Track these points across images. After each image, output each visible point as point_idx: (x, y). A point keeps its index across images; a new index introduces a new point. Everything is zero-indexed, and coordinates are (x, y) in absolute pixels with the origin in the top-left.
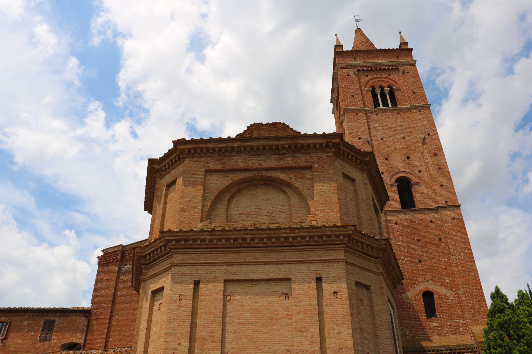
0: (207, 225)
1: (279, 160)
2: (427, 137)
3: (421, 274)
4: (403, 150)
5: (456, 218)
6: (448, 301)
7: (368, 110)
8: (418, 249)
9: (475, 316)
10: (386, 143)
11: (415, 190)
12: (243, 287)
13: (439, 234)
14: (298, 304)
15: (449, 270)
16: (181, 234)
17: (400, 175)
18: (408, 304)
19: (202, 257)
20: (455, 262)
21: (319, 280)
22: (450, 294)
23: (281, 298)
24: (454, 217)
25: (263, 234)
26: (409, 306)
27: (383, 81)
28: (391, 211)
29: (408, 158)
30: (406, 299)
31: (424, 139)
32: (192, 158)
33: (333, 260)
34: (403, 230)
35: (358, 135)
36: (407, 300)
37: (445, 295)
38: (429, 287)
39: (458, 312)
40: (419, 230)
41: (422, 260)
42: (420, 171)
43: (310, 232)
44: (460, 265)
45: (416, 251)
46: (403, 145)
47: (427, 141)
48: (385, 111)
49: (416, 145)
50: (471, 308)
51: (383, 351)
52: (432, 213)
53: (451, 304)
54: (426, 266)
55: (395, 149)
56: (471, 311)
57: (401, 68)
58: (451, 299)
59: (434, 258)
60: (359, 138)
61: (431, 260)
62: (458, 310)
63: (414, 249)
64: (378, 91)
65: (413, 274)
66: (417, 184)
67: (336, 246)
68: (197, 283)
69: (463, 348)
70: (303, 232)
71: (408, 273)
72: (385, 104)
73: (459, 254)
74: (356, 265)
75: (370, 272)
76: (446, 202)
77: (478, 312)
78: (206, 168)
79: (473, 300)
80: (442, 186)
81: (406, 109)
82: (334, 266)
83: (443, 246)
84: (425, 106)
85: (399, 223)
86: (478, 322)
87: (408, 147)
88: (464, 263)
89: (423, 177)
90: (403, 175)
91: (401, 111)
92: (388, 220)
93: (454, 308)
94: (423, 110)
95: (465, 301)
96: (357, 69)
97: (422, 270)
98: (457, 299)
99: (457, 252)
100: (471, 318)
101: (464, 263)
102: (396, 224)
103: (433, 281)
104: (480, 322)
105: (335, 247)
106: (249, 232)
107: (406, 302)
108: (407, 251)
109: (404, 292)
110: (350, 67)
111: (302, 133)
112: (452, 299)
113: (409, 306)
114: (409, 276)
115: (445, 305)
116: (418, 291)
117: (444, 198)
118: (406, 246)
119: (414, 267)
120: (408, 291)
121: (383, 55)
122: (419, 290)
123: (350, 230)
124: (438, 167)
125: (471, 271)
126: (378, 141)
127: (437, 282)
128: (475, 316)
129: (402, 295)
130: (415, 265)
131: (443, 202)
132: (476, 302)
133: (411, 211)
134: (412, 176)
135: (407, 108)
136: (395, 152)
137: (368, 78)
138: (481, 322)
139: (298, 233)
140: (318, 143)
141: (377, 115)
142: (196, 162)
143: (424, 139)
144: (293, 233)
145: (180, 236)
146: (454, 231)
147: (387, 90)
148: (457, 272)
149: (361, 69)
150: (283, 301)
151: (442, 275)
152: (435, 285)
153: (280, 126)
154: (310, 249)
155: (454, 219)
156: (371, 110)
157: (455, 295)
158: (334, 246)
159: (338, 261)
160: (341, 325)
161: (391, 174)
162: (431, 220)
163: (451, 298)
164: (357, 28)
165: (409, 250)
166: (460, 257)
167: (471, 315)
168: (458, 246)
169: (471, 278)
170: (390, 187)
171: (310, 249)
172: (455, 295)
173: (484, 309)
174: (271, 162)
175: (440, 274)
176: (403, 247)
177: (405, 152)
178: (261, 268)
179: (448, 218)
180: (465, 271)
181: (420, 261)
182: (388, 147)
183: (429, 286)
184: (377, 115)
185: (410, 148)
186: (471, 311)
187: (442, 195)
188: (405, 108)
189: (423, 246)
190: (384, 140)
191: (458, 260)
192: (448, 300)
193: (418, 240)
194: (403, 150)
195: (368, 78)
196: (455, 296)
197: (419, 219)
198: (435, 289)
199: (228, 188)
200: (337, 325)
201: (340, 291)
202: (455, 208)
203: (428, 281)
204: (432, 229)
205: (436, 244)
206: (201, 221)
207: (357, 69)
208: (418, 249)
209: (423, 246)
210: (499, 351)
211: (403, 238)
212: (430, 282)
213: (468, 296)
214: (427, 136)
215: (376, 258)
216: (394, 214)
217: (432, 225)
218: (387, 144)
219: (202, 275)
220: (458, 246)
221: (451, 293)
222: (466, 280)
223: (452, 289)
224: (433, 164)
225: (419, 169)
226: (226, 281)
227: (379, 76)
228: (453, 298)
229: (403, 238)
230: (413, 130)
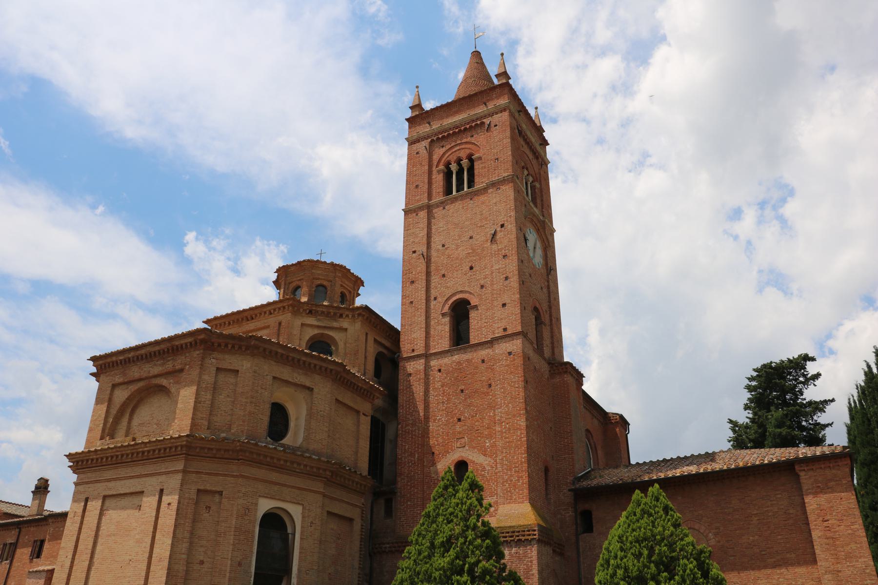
0: (108, 443)
1: (163, 365)
2: (500, 230)
3: (457, 439)
4: (467, 257)
5: (513, 352)
6: (483, 473)
7: (433, 204)
8: (460, 403)
9: (510, 491)
10: (448, 251)
11: (473, 316)
12: (115, 501)
13: (490, 379)
14: (143, 516)
15: (493, 429)
16: (78, 456)
17: (454, 299)
18: (435, 479)
19: (94, 475)
20: (499, 418)
21: (162, 491)
22: (487, 462)
23: (136, 511)
24: (510, 351)
25: (128, 450)
26: (436, 482)
27: (463, 148)
28: (435, 354)
29: (471, 268)
30: (434, 473)
31: (494, 235)
32: (106, 373)
33: (174, 471)
34: (446, 378)
35: (413, 248)
36: (436, 474)
37: (481, 465)
38: (463, 454)
39: (492, 486)
40: (465, 376)
41: (462, 418)
42: (482, 287)
43: (157, 445)
44: (504, 421)
45: (456, 406)
46: (468, 249)
47: (499, 236)
48: (463, 198)
49: (485, 245)
50: (507, 481)
51: (221, 558)
52: (486, 348)
53: (486, 477)
54: (466, 425)
55: (457, 259)
56: (506, 486)
57: (487, 121)
58: (487, 469)
59: (476, 414)
60: (414, 252)
61: (473, 417)
62: (493, 484)
63: (455, 404)
64: (454, 167)
65: (449, 439)
66: (476, 307)
67: (178, 457)
68: (87, 500)
69: (505, 531)
70: (153, 446)
71: (443, 438)
72: (460, 188)
73: (506, 406)
74: (203, 472)
75: (226, 476)
76: (505, 330)
77: (514, 486)
78: (113, 383)
79: (511, 470)
80: (504, 305)
81: (481, 190)
82: (174, 477)
83: (492, 395)
84: (505, 178)
85: (443, 369)
86: (512, 499)
87: (474, 250)
88: (510, 418)
89: (485, 294)
90: (461, 297)
91: (475, 195)
92: (431, 367)
93: (488, 481)
94: (502, 185)
95: (501, 472)
96: (430, 139)
97: (460, 433)
98: (494, 469)
99: (504, 404)
100: (504, 494)
101: (510, 418)
102: (440, 371)
103: (470, 447)
104: (514, 499)
105: (178, 458)
106: (118, 449)
107: (433, 477)
108: (446, 408)
109: (434, 464)
110: (422, 139)
111: (160, 339)
112: (489, 470)
113: (436, 482)
114: (442, 442)
115: (479, 478)
116: (450, 461)
117: (503, 324)
118: (446, 401)
119: (450, 428)
120: (439, 462)
121: (468, 106)
122: (451, 459)
123: (184, 441)
124: (504, 276)
125: (518, 429)
126: (438, 250)
127: (474, 448)
128: (510, 491)
129: (431, 468)
130: (451, 426)
131: (501, 330)
132: (514, 472)
133: (465, 348)
134: (471, 296)
135: (483, 187)
136: (456, 263)
137: (444, 149)
138: (515, 499)
139: (150, 447)
140: (272, 309)
141: (444, 208)
142: (107, 376)
143: (494, 235)
144: (147, 447)
145: (77, 458)
146: (507, 372)
147: (465, 163)
148: (499, 432)
149: (435, 138)
150: (136, 513)
151: (482, 437)
152: (471, 452)
153: (306, 264)
154: (162, 460)
155: (510, 353)
156: (436, 202)
157: (493, 463)
158: (176, 457)
159: (176, 472)
160: (166, 536)
161: (445, 299)
162: (483, 359)
163: (488, 468)
164: (474, 50)
165: (449, 405)
166: (507, 410)
167: (505, 490)
168: (507, 394)
169: (515, 439)
170: (441, 317)
171: (162, 460)
172: (493, 463)
173: (523, 482)
174: (156, 370)
175: (480, 437)
176: (443, 402)
177: (468, 260)
178: (127, 482)
179: (502, 354)
180: (509, 429)
181: (459, 420)
182: (449, 256)
183: (464, 454)
184: (444, 208)
185: (477, 253)
186: (506, 486)
187: (501, 319)
188: (480, 188)
189: (466, 399)
190: (446, 247)
191: (503, 415)
192: (483, 471)
193: (462, 391)
194: (467, 257)
195: (444, 149)
196: (493, 465)
197: (468, 361)
198: (470, 457)
199: (129, 399)
200: (164, 535)
201: (173, 502)
202: (515, 337)
203: (464, 447)
204: (482, 373)
205: (483, 393)
206: (101, 439)
207: (430, 139)
208: (460, 403)
209: (466, 399)
210: (404, 553)
211: (444, 390)
212: (467, 448)
213: (507, 465)
214: (499, 229)
215: (238, 460)
216: (439, 357)
217: (483, 367)
218: (449, 253)
219: (91, 492)
220: (507, 394)
221: (489, 462)
222: (508, 442)
223: (491, 456)
224: (499, 272)
225: (482, 282)
226: (105, 498)
227: (458, 142)
228: (490, 468)
229: (444, 390)
230: (486, 222)
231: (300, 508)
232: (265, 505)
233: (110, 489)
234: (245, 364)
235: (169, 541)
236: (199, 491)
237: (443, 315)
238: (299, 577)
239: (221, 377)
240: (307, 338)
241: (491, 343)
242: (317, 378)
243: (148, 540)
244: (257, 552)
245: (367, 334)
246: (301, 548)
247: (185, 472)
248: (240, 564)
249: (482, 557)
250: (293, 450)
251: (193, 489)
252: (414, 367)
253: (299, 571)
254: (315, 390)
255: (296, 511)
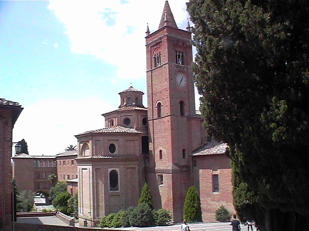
1: (86, 139)
174: (86, 140)
231: (119, 169)
232: (110, 170)
233: (110, 138)
234: (101, 138)
235: (92, 180)
236: (96, 169)
237: (156, 107)
238: (120, 184)
239: (97, 142)
240: (123, 119)
241: (164, 117)
242: (119, 137)
243: (89, 179)
244: (53, 225)
245: (138, 115)
246: (120, 178)
247: (153, 120)
248: (106, 183)
249: (253, 107)
250: (116, 156)
251: (95, 169)
252: (150, 123)
253: (120, 182)
254: (119, 140)
255: (118, 170)
